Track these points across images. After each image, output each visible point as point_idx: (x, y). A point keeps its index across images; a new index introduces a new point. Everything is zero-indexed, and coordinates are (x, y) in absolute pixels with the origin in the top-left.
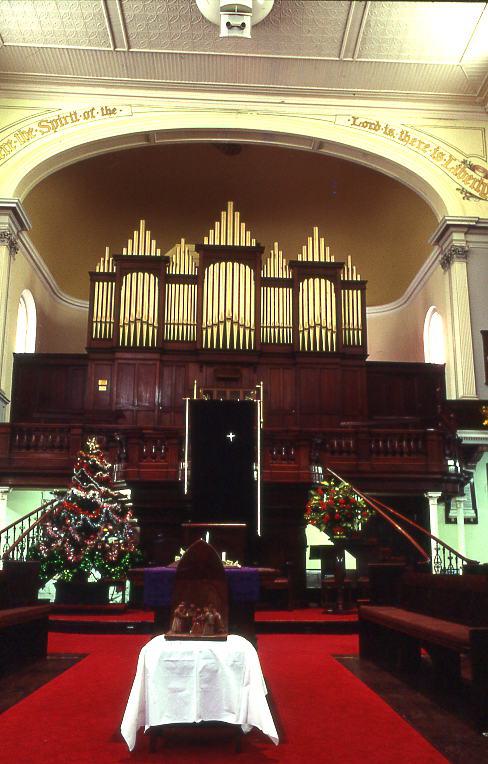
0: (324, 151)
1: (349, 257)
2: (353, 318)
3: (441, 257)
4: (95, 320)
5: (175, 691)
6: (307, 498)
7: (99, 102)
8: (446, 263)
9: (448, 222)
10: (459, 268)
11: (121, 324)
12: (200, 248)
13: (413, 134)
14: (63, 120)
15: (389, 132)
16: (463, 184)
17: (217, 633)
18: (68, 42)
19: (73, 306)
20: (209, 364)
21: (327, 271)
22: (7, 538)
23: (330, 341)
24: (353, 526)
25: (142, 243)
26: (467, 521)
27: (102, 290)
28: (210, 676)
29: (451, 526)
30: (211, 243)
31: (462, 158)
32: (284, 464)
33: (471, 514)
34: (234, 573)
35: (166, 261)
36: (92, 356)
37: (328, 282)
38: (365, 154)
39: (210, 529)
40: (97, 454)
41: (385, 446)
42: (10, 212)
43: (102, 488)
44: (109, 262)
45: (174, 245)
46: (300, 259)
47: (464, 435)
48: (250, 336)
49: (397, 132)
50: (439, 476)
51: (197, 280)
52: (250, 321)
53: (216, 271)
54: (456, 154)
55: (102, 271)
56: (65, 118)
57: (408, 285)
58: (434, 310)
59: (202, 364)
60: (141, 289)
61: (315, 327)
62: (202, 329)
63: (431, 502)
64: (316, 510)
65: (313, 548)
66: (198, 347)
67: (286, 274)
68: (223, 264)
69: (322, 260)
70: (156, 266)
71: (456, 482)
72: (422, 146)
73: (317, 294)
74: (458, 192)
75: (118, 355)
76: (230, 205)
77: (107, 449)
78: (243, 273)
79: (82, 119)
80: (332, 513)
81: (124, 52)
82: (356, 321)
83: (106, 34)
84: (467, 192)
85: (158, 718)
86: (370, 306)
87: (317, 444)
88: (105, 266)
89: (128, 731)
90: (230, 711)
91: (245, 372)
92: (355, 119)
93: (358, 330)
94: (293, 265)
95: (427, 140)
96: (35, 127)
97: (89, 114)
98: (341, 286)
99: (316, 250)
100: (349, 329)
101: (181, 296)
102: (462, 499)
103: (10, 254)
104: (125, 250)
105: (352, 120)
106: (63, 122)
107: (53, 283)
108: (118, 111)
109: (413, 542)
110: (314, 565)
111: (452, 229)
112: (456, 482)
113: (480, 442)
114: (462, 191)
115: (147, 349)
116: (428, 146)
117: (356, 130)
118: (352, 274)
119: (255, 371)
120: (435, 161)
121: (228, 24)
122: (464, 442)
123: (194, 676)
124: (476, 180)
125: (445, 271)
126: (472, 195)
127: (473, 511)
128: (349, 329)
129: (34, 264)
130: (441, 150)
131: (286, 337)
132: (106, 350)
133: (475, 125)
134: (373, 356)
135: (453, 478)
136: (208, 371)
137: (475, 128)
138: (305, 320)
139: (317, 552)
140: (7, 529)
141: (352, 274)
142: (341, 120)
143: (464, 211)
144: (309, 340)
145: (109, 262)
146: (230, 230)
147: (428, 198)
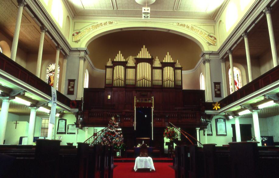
0: (170, 32)
1: (177, 61)
2: (179, 78)
3: (203, 60)
6: (164, 131)
8: (204, 63)
10: (207, 65)
11: (114, 80)
12: (136, 59)
15: (188, 27)
17: (147, 156)
19: (99, 71)
21: (172, 65)
22: (90, 140)
23: (172, 84)
24: (174, 137)
25: (120, 58)
26: (208, 135)
27: (109, 70)
28: (146, 162)
30: (139, 57)
32: (159, 122)
34: (148, 148)
35: (126, 62)
37: (172, 68)
38: (181, 33)
39: (144, 140)
40: (114, 121)
41: (187, 115)
42: (84, 51)
44: (110, 62)
45: (128, 57)
46: (164, 61)
47: (207, 112)
51: (135, 68)
52: (150, 78)
53: (140, 65)
54: (206, 33)
55: (108, 65)
56: (99, 25)
58: (202, 74)
61: (168, 81)
62: (136, 81)
63: (197, 130)
64: (166, 134)
65: (166, 143)
67: (160, 66)
68: (142, 63)
70: (124, 64)
71: (204, 125)
72: (197, 31)
73: (169, 72)
74: (207, 44)
75: (114, 89)
77: (116, 120)
78: (148, 65)
82: (179, 78)
83: (111, 6)
85: (139, 167)
87: (167, 117)
88: (109, 64)
89: (135, 169)
90: (149, 166)
91: (149, 93)
92: (178, 23)
93: (180, 81)
94: (162, 63)
96: (91, 27)
97: (105, 24)
98: (175, 69)
99: (168, 59)
101: (131, 72)
104: (115, 59)
107: (93, 66)
108: (113, 22)
110: (166, 147)
111: (205, 54)
112: (204, 125)
113: (211, 114)
114: (208, 43)
116: (198, 31)
117: (179, 27)
118: (178, 66)
122: (207, 114)
123: (144, 162)
124: (212, 40)
130: (202, 32)
132: (110, 87)
133: (211, 24)
134: (184, 88)
135: (203, 124)
139: (167, 144)
142: (175, 24)
143: (209, 49)
144: (167, 84)
145: (110, 62)
146: (144, 53)
147: (199, 44)
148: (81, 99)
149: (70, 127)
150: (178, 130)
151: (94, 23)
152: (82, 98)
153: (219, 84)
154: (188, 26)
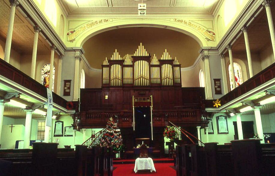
2: (177, 75)
3: (202, 57)
4: (103, 78)
5: (141, 165)
7: (103, 19)
8: (203, 59)
9: (203, 48)
10: (206, 61)
11: (111, 79)
13: (192, 23)
14: (93, 24)
15: (185, 23)
16: (207, 37)
17: (147, 157)
18: (96, 6)
19: (96, 71)
20: (137, 90)
23: (171, 83)
25: (116, 56)
27: (105, 70)
28: (146, 163)
29: (205, 135)
30: (136, 55)
31: (206, 29)
32: (158, 122)
33: (212, 131)
34: (148, 148)
36: (103, 89)
37: (170, 65)
38: (179, 29)
39: (143, 140)
40: (112, 121)
42: (80, 50)
43: (114, 130)
45: (125, 55)
46: (161, 59)
48: (148, 82)
49: (188, 22)
50: (200, 122)
51: (132, 66)
54: (204, 28)
55: (105, 64)
56: (94, 23)
57: (194, 62)
58: (202, 71)
59: (134, 90)
60: (116, 69)
64: (166, 133)
66: (133, 85)
67: (158, 63)
69: (168, 59)
70: (121, 62)
72: (195, 26)
73: (167, 69)
74: (206, 39)
75: (111, 88)
76: (141, 44)
78: (145, 63)
79: (99, 23)
80: (169, 134)
81: (111, 7)
84: (208, 39)
85: (139, 169)
86: (182, 67)
88: (106, 63)
89: (135, 170)
90: (149, 167)
91: (147, 92)
92: (176, 19)
95: (195, 24)
96: (86, 26)
97: (101, 22)
98: (174, 66)
99: (166, 56)
100: (176, 78)
101: (128, 71)
102: (207, 128)
103: (80, 61)
104: (111, 58)
105: (175, 20)
106: (94, 24)
107: (89, 65)
108: (109, 20)
109: (191, 140)
110: (166, 147)
111: (204, 50)
114: (207, 39)
115: (119, 87)
116: (196, 26)
117: (177, 23)
118: (177, 63)
119: (150, 92)
120: (198, 30)
121: (140, 13)
123: (144, 163)
125: (203, 62)
126: (210, 40)
127: (212, 130)
128: (176, 78)
129: (84, 62)
131: (159, 81)
132: (107, 87)
133: (209, 19)
134: (184, 85)
136: (136, 92)
137: (210, 21)
138: (163, 76)
139: (167, 144)
140: (88, 140)
141: (177, 63)
142: (172, 20)
143: (208, 45)
144: (165, 82)
148: (77, 100)
149: (67, 129)
150: (178, 129)
151: (89, 21)
152: (79, 99)
153: (219, 80)
154: (186, 21)
